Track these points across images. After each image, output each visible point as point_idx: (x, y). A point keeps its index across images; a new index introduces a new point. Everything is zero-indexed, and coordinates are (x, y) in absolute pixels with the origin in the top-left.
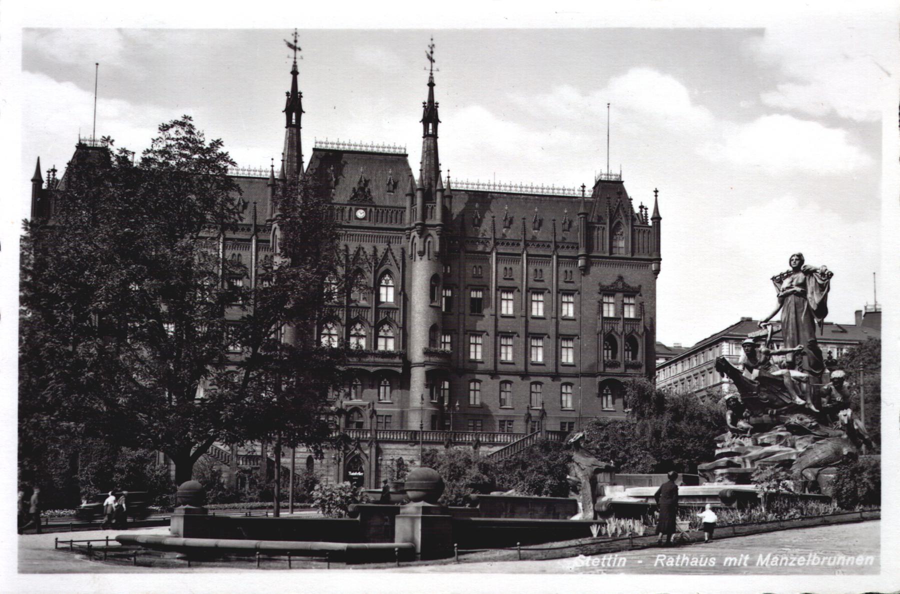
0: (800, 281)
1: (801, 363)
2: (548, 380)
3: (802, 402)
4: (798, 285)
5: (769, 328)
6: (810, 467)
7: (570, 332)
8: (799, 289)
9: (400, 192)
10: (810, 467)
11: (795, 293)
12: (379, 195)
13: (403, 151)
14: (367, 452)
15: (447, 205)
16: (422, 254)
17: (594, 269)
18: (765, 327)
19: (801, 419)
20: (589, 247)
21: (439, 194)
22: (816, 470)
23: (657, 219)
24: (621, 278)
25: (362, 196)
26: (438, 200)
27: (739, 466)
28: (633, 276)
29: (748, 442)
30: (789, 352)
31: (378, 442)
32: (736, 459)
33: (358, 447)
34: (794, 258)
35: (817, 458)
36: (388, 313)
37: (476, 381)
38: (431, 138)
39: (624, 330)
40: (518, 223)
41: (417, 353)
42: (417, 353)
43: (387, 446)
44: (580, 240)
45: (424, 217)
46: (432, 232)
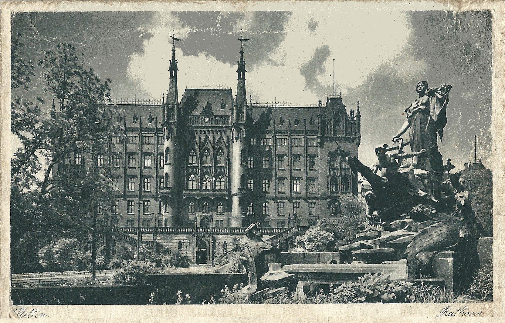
0: (424, 101)
1: (424, 163)
2: (302, 201)
3: (424, 194)
4: (423, 104)
5: (400, 141)
6: (423, 250)
7: (314, 176)
8: (423, 107)
9: (227, 109)
10: (423, 250)
11: (420, 111)
12: (217, 110)
13: (229, 88)
14: (208, 239)
15: (250, 113)
16: (237, 139)
17: (326, 145)
18: (397, 140)
19: (423, 208)
20: (323, 132)
21: (245, 108)
22: (430, 254)
23: (359, 116)
24: (339, 147)
25: (208, 111)
26: (245, 111)
27: (372, 247)
28: (346, 147)
29: (380, 228)
30: (414, 155)
31: (213, 234)
32: (370, 243)
33: (204, 237)
34: (420, 84)
35: (432, 241)
36: (221, 169)
37: (266, 202)
38: (242, 80)
39: (341, 174)
40: (287, 122)
41: (235, 189)
42: (235, 189)
43: (218, 236)
44: (318, 129)
45: (237, 120)
46: (242, 127)
